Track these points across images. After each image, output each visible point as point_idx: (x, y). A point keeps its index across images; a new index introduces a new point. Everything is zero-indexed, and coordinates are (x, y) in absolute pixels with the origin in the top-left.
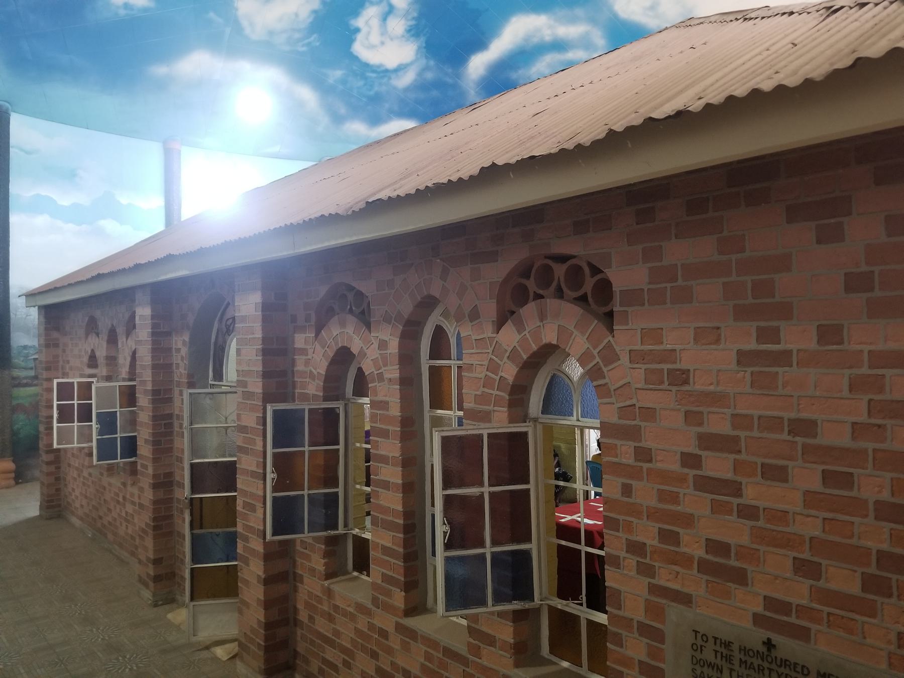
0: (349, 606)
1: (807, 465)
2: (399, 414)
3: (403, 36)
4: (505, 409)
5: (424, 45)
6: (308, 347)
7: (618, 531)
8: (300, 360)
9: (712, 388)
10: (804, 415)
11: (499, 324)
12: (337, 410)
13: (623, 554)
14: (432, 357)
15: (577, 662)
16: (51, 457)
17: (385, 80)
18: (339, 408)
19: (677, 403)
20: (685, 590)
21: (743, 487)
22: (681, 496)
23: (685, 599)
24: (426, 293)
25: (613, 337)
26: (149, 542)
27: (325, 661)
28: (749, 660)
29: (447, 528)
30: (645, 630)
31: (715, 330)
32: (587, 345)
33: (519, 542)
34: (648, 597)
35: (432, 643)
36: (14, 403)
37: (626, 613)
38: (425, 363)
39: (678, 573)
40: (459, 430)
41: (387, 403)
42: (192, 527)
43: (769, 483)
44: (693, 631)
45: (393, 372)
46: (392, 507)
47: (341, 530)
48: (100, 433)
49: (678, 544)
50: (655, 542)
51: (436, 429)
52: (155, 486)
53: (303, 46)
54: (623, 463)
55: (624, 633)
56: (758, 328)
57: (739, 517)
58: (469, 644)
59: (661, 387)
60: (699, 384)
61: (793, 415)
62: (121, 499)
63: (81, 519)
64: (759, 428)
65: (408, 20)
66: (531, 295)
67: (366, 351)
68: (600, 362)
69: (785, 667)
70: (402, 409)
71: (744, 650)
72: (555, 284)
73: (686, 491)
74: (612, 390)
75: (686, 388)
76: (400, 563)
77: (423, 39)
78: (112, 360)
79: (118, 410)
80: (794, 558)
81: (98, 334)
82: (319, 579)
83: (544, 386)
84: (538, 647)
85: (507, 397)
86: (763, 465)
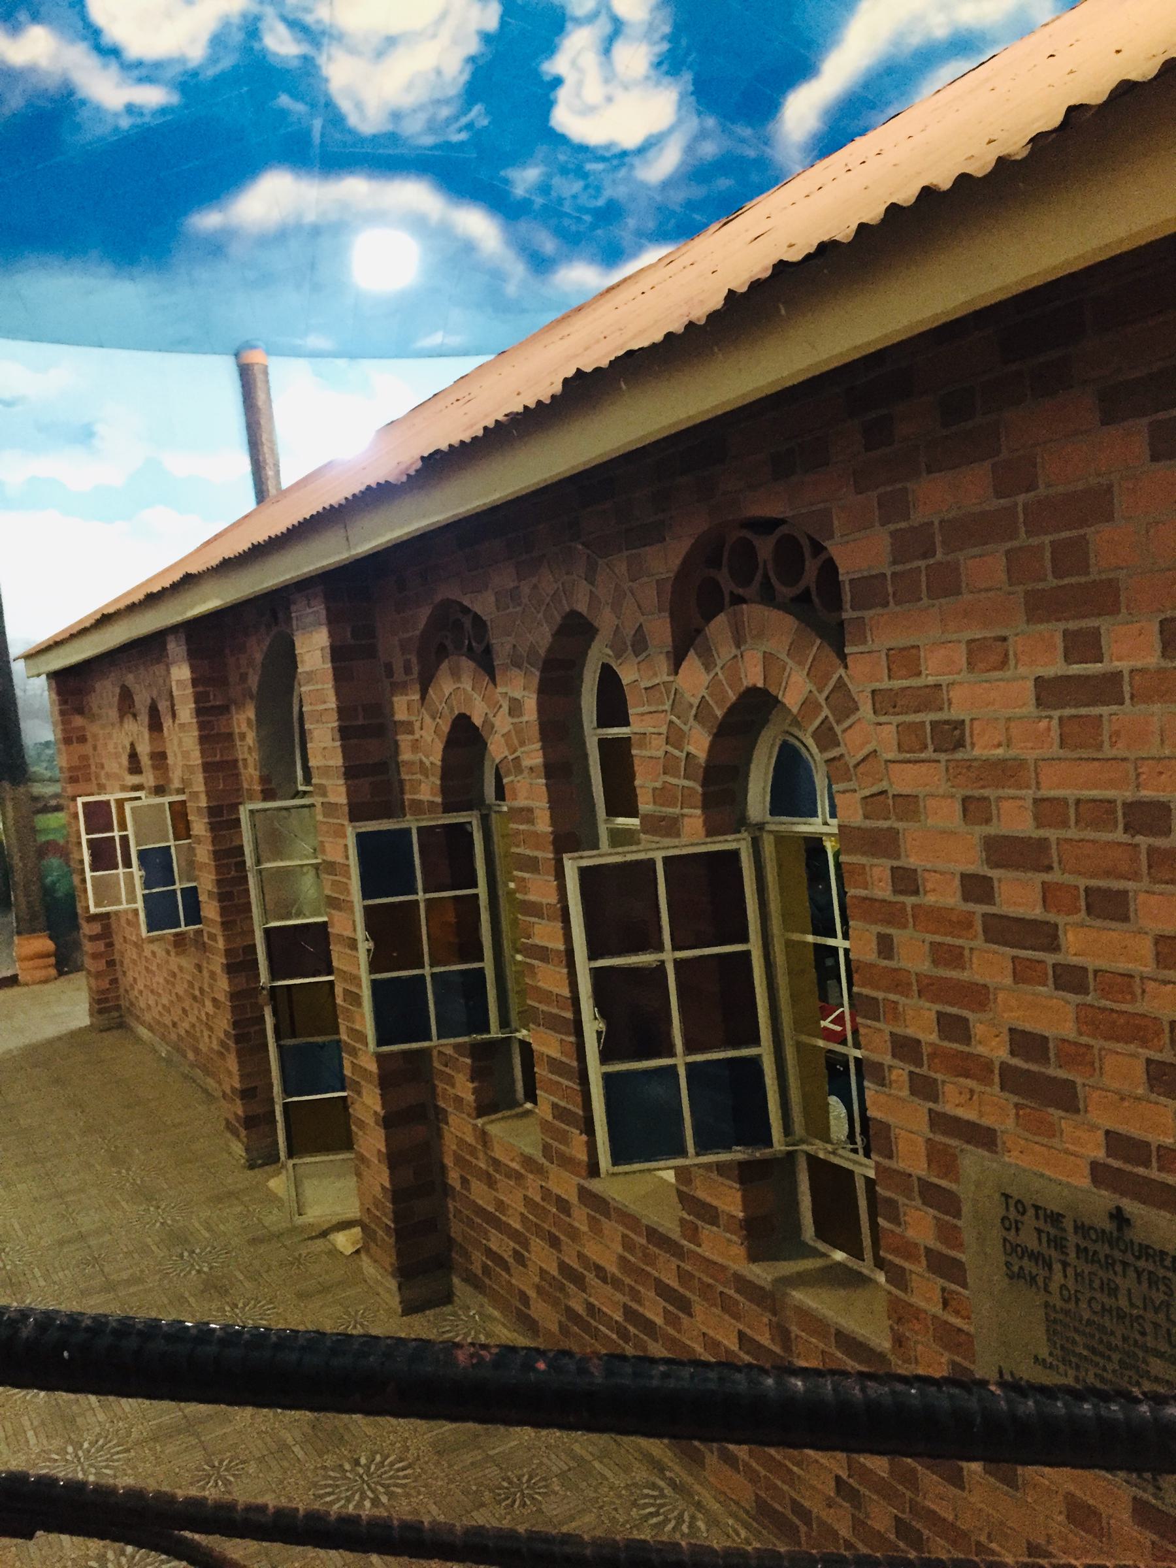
0: (512, 1160)
1: (1159, 888)
2: (550, 829)
3: (647, 78)
4: (698, 812)
5: (691, 88)
6: (413, 718)
7: (878, 1020)
8: (404, 740)
9: (1000, 751)
10: (1146, 794)
11: (677, 661)
12: (468, 827)
13: (888, 1060)
14: (603, 722)
15: (858, 1254)
16: (96, 928)
17: (622, 173)
18: (470, 823)
19: (949, 784)
20: (986, 1122)
21: (1060, 933)
22: (967, 952)
23: (984, 1138)
24: (568, 609)
25: (846, 667)
26: (232, 1063)
27: (489, 1252)
28: (1092, 1247)
29: (601, 1026)
30: (932, 1195)
31: (999, 643)
32: (810, 686)
33: (736, 1045)
34: (931, 1136)
35: (628, 1219)
36: (42, 839)
37: (900, 1165)
38: (592, 735)
39: (972, 1091)
40: (611, 854)
41: (530, 810)
42: (278, 1036)
43: (1098, 923)
44: (1003, 1194)
45: (533, 756)
46: (556, 990)
47: (495, 1033)
48: (147, 884)
49: (967, 1039)
50: (933, 1037)
51: (570, 855)
52: (231, 969)
53: (460, 130)
54: (876, 897)
55: (901, 1200)
56: (1066, 633)
57: (1057, 987)
58: (682, 1221)
59: (923, 755)
60: (984, 747)
61: (1128, 795)
62: (197, 993)
63: (150, 1028)
64: (1077, 822)
65: (655, 43)
66: (727, 599)
67: (493, 719)
68: (830, 716)
69: (1147, 1260)
70: (554, 821)
71: (1082, 1229)
72: (758, 577)
73: (973, 944)
74: (851, 765)
75: (959, 755)
76: (575, 1087)
77: (688, 76)
78: (159, 758)
79: (171, 843)
80: (1149, 1061)
81: (135, 716)
82: (469, 1115)
83: (768, 764)
84: (797, 1227)
85: (700, 789)
86: (1087, 889)
